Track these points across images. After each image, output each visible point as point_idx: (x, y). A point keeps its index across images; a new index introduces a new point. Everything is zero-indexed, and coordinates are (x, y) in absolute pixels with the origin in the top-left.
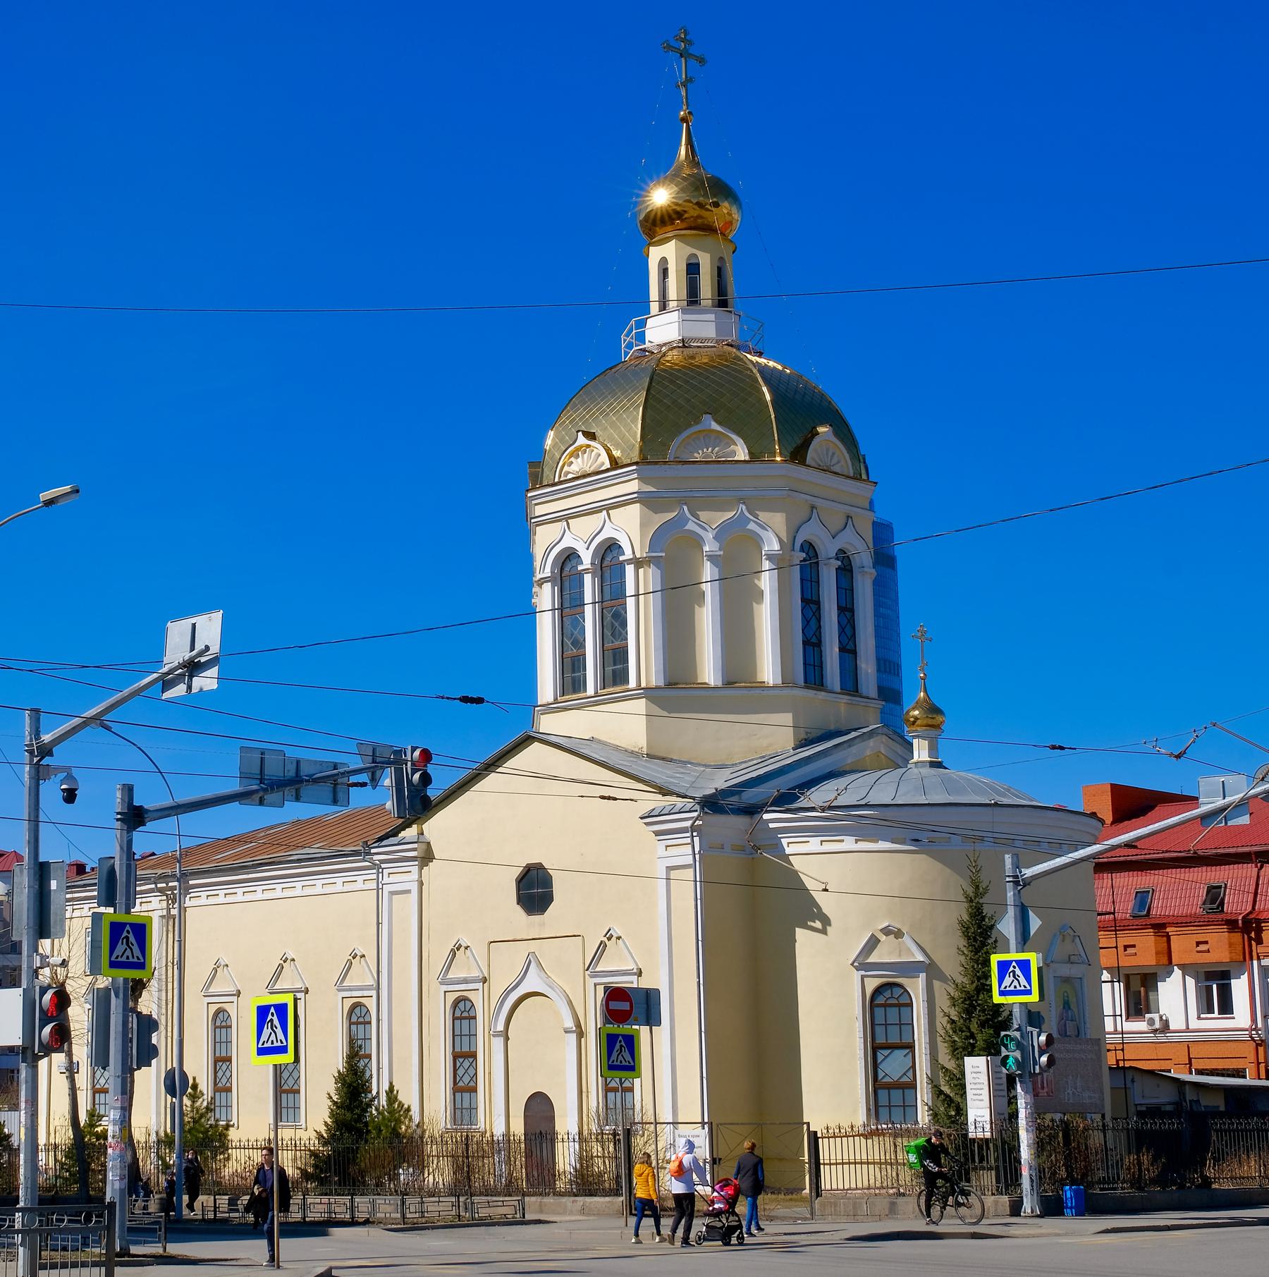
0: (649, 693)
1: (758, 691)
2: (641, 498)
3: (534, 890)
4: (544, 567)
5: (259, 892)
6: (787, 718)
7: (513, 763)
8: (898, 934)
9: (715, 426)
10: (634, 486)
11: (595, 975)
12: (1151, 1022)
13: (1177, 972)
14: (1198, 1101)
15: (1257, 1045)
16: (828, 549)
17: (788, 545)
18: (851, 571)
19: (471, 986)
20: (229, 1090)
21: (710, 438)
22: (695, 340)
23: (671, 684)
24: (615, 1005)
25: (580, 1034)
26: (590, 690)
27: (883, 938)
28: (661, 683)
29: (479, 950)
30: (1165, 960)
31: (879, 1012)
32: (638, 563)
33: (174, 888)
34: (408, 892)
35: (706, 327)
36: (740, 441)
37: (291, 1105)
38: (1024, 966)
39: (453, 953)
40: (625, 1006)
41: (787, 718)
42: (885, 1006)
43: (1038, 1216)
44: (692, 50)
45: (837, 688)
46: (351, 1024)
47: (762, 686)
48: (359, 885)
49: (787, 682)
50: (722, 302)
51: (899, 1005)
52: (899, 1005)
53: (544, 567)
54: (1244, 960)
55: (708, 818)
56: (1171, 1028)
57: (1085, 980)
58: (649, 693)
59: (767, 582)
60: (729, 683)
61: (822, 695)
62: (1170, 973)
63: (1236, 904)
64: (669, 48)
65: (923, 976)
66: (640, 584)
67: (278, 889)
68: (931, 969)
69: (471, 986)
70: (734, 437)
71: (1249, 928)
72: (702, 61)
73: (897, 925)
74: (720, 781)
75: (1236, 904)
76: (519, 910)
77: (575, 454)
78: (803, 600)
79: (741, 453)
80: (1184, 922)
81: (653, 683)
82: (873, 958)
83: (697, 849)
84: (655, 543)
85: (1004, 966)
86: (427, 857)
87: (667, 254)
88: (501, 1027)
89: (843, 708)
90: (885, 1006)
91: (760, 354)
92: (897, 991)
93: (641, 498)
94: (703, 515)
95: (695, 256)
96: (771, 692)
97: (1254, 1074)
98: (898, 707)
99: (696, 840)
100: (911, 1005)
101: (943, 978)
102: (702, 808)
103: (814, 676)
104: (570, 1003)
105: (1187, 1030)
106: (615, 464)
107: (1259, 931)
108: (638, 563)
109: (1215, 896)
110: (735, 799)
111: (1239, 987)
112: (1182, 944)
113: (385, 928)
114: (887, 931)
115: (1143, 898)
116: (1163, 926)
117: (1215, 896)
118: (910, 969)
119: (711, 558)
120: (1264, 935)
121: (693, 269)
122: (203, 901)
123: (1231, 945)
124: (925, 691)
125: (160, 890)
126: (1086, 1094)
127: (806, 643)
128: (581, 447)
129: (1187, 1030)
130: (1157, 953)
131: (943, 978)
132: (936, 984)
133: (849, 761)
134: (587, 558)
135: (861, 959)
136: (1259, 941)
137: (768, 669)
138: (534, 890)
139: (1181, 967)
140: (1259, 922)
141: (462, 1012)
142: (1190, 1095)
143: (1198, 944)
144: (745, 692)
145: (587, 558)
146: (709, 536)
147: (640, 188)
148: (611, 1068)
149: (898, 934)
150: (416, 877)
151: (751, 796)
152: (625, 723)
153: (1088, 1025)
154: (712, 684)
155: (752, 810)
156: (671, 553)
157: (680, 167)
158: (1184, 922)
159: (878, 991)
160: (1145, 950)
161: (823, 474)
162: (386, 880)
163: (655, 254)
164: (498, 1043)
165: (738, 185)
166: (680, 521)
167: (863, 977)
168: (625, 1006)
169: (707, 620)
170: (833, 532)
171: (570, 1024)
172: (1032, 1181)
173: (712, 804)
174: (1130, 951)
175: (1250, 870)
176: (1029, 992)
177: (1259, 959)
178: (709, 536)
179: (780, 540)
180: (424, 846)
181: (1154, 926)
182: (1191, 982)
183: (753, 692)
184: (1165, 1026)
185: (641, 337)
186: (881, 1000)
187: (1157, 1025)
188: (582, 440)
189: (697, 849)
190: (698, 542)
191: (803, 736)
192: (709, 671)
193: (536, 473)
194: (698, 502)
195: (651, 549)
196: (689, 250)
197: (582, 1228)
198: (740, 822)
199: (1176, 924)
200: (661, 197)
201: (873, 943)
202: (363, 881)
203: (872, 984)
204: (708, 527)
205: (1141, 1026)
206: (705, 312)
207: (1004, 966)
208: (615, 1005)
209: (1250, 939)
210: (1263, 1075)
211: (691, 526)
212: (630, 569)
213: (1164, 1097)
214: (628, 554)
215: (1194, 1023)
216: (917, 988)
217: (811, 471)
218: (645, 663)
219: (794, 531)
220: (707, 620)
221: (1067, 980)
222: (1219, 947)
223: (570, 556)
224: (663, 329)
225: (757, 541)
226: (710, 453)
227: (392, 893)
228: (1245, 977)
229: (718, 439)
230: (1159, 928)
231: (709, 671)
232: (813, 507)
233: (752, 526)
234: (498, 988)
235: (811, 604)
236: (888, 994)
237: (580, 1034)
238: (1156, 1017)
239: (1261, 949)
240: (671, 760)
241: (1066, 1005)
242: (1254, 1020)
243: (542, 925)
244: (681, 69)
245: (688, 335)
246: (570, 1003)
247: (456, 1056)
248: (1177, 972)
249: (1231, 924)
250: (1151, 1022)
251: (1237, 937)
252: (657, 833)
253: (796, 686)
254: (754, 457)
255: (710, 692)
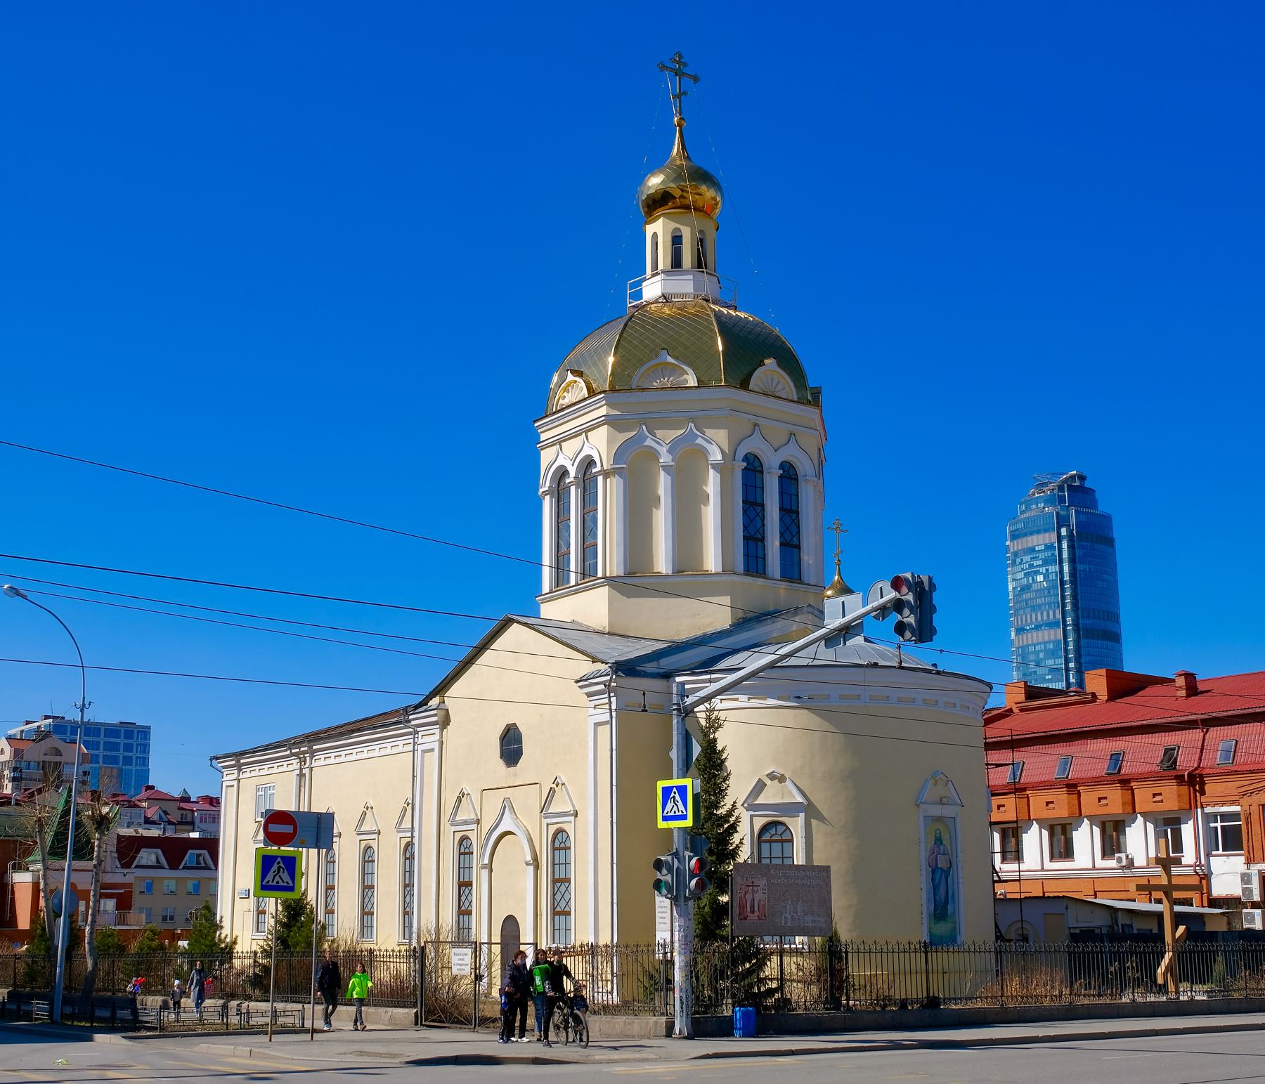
0: (610, 581)
1: (701, 578)
2: (609, 420)
3: (511, 746)
4: (546, 484)
5: (354, 754)
6: (727, 600)
7: (498, 644)
8: (782, 779)
9: (670, 359)
10: (603, 411)
11: (548, 816)
12: (1120, 860)
13: (1140, 819)
14: (1131, 925)
15: (1201, 879)
16: (772, 462)
17: (730, 457)
18: (797, 479)
19: (469, 827)
20: (470, 913)
21: (666, 369)
22: (677, 295)
23: (629, 574)
24: (273, 828)
25: (537, 867)
26: (573, 582)
27: (768, 782)
28: (622, 573)
29: (475, 797)
30: (1130, 809)
31: (765, 847)
32: (606, 474)
33: (304, 752)
34: (432, 750)
35: (685, 285)
36: (690, 371)
37: (563, 927)
38: (682, 790)
39: (459, 800)
40: (288, 829)
41: (727, 600)
42: (770, 841)
43: (685, 1038)
44: (685, 70)
45: (778, 575)
46: (554, 849)
47: (707, 574)
48: (400, 749)
49: (727, 569)
50: (700, 263)
51: (782, 841)
52: (782, 841)
53: (546, 484)
54: (1189, 809)
55: (620, 680)
56: (1136, 864)
57: (958, 820)
58: (610, 581)
59: (712, 485)
60: (678, 572)
61: (760, 581)
62: (1134, 820)
63: (1186, 762)
64: (663, 67)
65: (802, 815)
66: (609, 494)
67: (365, 752)
68: (809, 810)
69: (469, 827)
70: (686, 368)
71: (1195, 782)
72: (696, 79)
73: (780, 771)
74: (631, 651)
75: (1186, 762)
76: (501, 762)
77: (566, 390)
78: (781, 509)
79: (692, 381)
80: (1143, 778)
81: (615, 574)
82: (761, 800)
83: (614, 707)
84: (618, 457)
85: (667, 791)
86: (445, 722)
87: (658, 229)
88: (486, 861)
89: (782, 593)
90: (770, 841)
91: (735, 309)
92: (781, 829)
93: (609, 420)
94: (659, 433)
95: (678, 229)
96: (713, 578)
97: (1199, 904)
98: (1110, 644)
99: (614, 700)
100: (792, 841)
101: (821, 818)
102: (615, 672)
103: (754, 564)
104: (530, 841)
105: (1094, 868)
106: (592, 392)
107: (1202, 784)
108: (606, 474)
109: (1170, 755)
110: (654, 664)
111: (1187, 830)
112: (1143, 796)
113: (418, 779)
114: (772, 776)
115: (1116, 759)
116: (1128, 781)
117: (1170, 755)
118: (791, 809)
119: (666, 468)
120: (1206, 787)
121: (677, 240)
122: (322, 762)
123: (1179, 796)
124: (840, 574)
125: (293, 755)
126: (809, 918)
127: (747, 538)
128: (570, 382)
129: (1094, 868)
130: (1123, 804)
131: (821, 818)
132: (814, 822)
133: (775, 635)
134: (572, 471)
135: (750, 801)
136: (1203, 793)
137: (712, 560)
138: (511, 746)
139: (1144, 814)
140: (1201, 776)
141: (464, 849)
142: (1122, 920)
143: (1154, 795)
144: (690, 579)
145: (572, 471)
146: (663, 450)
147: (641, 180)
148: (264, 888)
149: (782, 779)
150: (437, 737)
151: (667, 663)
152: (591, 607)
153: (960, 859)
154: (664, 572)
155: (668, 676)
156: (633, 467)
157: (675, 159)
158: (1143, 778)
159: (765, 828)
160: (1115, 799)
161: (765, 398)
162: (420, 741)
163: (650, 229)
164: (485, 873)
165: (719, 174)
166: (639, 439)
167: (752, 817)
168: (288, 829)
169: (661, 521)
170: (776, 446)
171: (529, 858)
172: (682, 1003)
173: (626, 668)
174: (1103, 802)
175: (1196, 735)
176: (684, 817)
177: (1202, 807)
178: (663, 450)
179: (723, 452)
180: (443, 712)
181: (1121, 782)
182: (1150, 827)
183: (697, 579)
184: (1131, 864)
185: (639, 295)
186: (766, 837)
187: (1124, 863)
188: (570, 377)
189: (614, 707)
190: (655, 455)
191: (740, 614)
192: (662, 563)
193: (543, 408)
194: (655, 422)
195: (615, 462)
196: (674, 225)
197: (395, 1035)
198: (659, 684)
199: (1137, 780)
200: (655, 181)
201: (760, 787)
202: (402, 745)
203: (759, 823)
204: (663, 442)
205: (1112, 863)
206: (686, 272)
207: (667, 791)
208: (273, 828)
209: (1195, 791)
210: (1205, 903)
211: (649, 442)
212: (600, 479)
213: (1098, 921)
214: (598, 468)
215: (1100, 863)
216: (797, 825)
217: (753, 395)
218: (610, 559)
219: (735, 445)
220: (661, 521)
221: (939, 819)
222: (1171, 796)
223: (563, 472)
224: (652, 289)
225: (704, 453)
226: (666, 381)
227: (424, 751)
228: (1191, 822)
229: (674, 370)
230: (1125, 782)
231: (662, 563)
232: (755, 425)
233: (700, 441)
234: (487, 825)
235: (753, 506)
236: (773, 831)
237: (537, 867)
238: (1123, 855)
239: (1204, 799)
240: (628, 637)
241: (938, 841)
242: (1198, 857)
243: (515, 775)
244: (671, 85)
245: (668, 291)
246: (530, 841)
247: (460, 886)
248: (1140, 819)
249: (1179, 779)
250: (1120, 860)
251: (1185, 789)
252: (589, 695)
253: (735, 573)
254: (702, 384)
255: (662, 580)
